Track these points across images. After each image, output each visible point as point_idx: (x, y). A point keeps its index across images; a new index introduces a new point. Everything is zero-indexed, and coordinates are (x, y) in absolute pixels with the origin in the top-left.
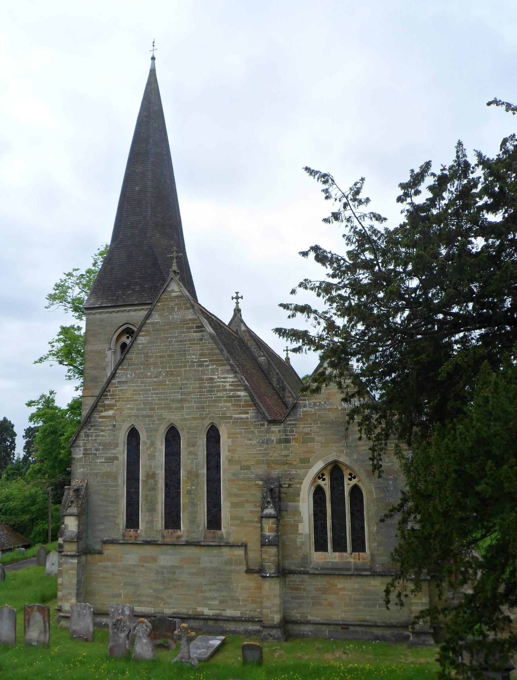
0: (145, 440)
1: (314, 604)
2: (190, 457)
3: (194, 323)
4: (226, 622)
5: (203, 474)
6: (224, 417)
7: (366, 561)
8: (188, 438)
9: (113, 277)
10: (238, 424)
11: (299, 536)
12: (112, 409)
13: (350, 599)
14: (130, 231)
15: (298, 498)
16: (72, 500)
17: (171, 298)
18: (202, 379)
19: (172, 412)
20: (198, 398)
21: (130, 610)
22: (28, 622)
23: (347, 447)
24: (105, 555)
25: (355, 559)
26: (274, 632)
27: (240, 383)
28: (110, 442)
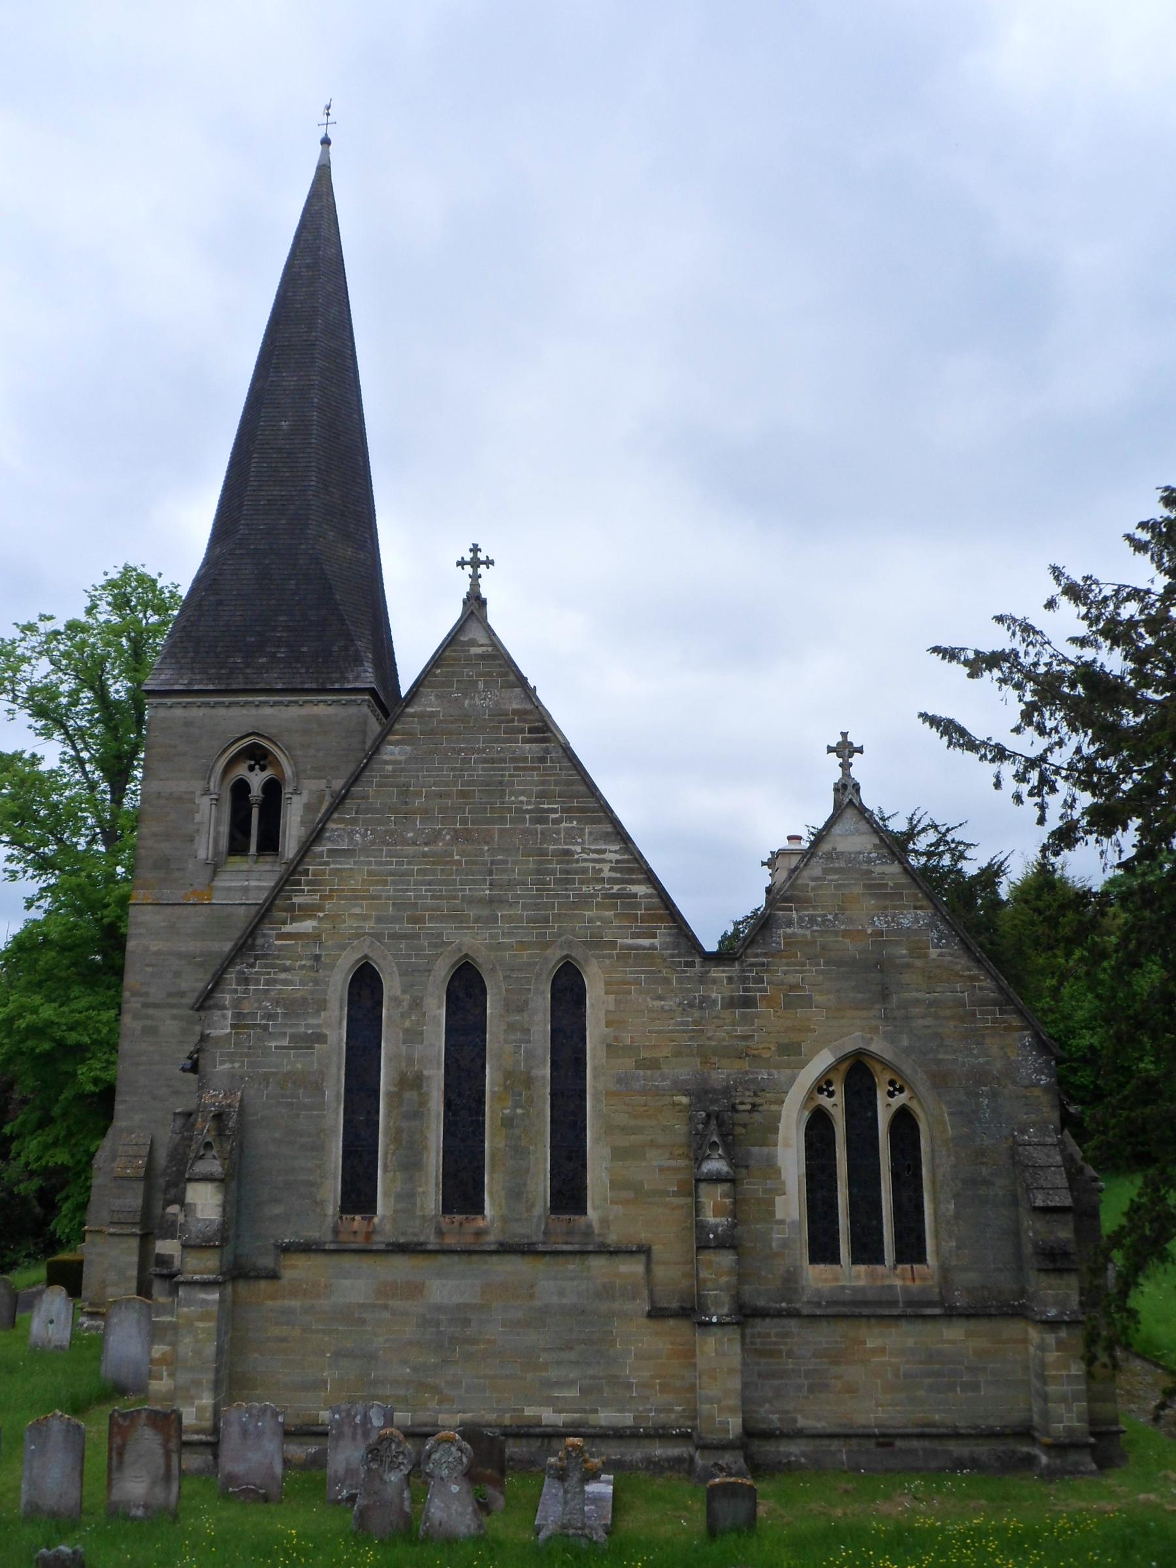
0: (399, 993)
1: (811, 1389)
2: (513, 1037)
3: (525, 721)
4: (597, 1441)
5: (544, 1077)
6: (596, 944)
7: (930, 1283)
8: (507, 990)
9: (222, 623)
10: (631, 961)
11: (776, 1227)
12: (311, 917)
13: (897, 1376)
14: (263, 520)
15: (774, 1136)
16: (209, 1139)
17: (469, 658)
18: (543, 853)
19: (468, 928)
20: (531, 897)
21: (384, 1416)
22: (121, 1454)
23: (886, 1018)
24: (284, 1281)
25: (904, 1279)
26: (727, 1459)
27: (636, 865)
28: (305, 999)
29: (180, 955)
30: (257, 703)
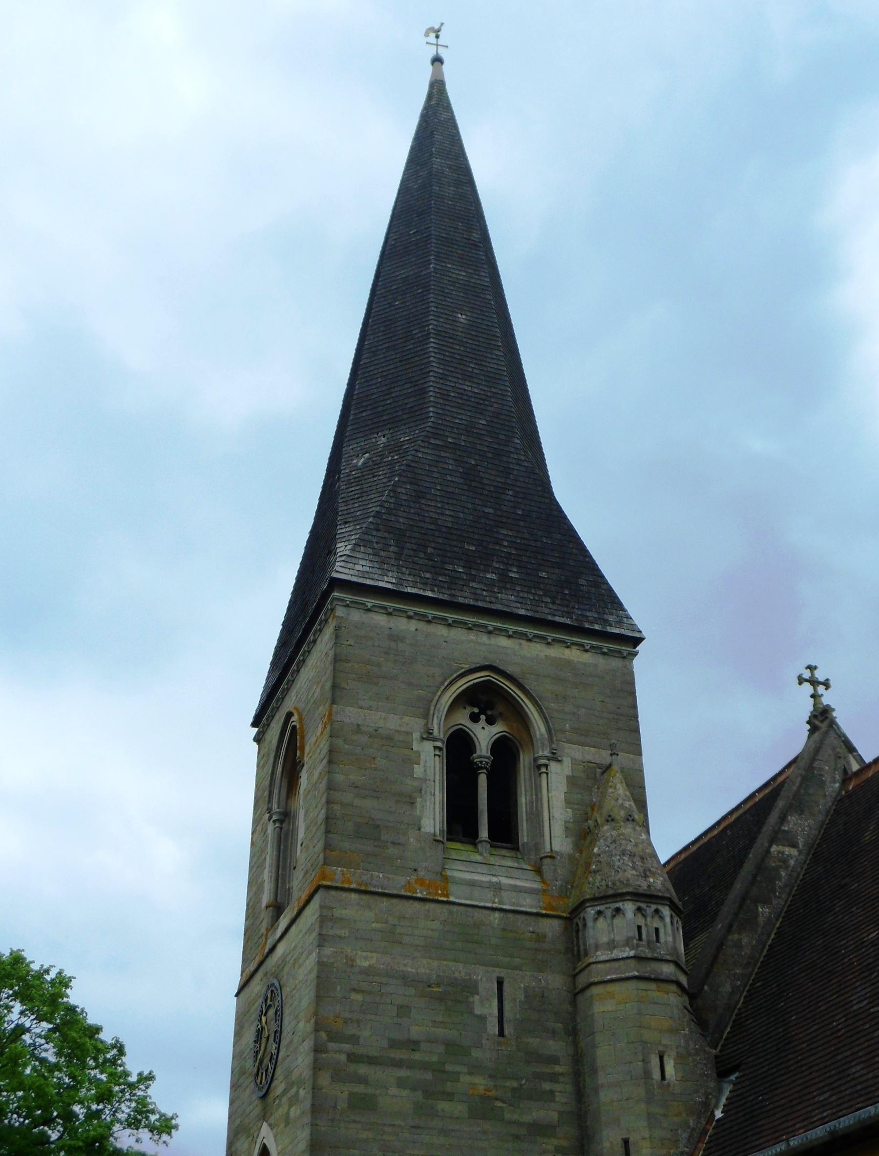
29: (406, 980)
30: (491, 628)
